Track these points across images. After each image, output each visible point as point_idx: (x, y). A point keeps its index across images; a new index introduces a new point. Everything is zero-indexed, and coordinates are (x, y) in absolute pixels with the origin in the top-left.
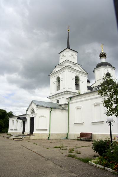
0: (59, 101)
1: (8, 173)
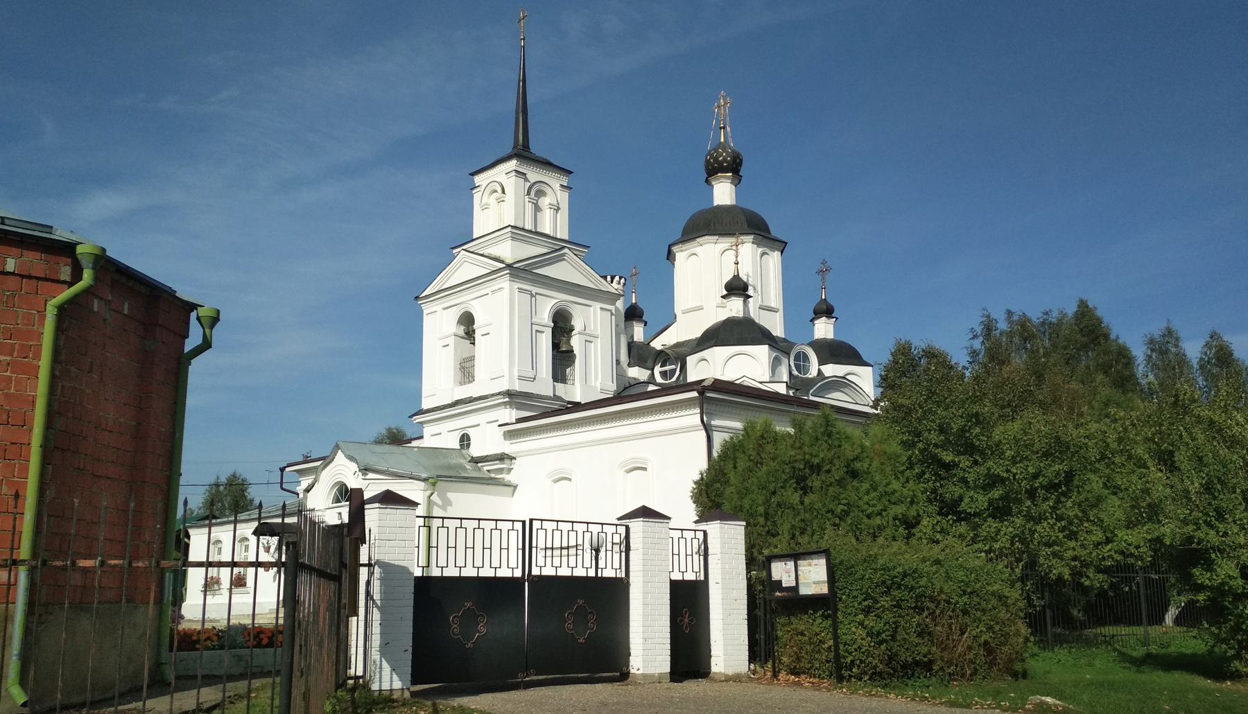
0: (469, 439)
1: (880, 435)
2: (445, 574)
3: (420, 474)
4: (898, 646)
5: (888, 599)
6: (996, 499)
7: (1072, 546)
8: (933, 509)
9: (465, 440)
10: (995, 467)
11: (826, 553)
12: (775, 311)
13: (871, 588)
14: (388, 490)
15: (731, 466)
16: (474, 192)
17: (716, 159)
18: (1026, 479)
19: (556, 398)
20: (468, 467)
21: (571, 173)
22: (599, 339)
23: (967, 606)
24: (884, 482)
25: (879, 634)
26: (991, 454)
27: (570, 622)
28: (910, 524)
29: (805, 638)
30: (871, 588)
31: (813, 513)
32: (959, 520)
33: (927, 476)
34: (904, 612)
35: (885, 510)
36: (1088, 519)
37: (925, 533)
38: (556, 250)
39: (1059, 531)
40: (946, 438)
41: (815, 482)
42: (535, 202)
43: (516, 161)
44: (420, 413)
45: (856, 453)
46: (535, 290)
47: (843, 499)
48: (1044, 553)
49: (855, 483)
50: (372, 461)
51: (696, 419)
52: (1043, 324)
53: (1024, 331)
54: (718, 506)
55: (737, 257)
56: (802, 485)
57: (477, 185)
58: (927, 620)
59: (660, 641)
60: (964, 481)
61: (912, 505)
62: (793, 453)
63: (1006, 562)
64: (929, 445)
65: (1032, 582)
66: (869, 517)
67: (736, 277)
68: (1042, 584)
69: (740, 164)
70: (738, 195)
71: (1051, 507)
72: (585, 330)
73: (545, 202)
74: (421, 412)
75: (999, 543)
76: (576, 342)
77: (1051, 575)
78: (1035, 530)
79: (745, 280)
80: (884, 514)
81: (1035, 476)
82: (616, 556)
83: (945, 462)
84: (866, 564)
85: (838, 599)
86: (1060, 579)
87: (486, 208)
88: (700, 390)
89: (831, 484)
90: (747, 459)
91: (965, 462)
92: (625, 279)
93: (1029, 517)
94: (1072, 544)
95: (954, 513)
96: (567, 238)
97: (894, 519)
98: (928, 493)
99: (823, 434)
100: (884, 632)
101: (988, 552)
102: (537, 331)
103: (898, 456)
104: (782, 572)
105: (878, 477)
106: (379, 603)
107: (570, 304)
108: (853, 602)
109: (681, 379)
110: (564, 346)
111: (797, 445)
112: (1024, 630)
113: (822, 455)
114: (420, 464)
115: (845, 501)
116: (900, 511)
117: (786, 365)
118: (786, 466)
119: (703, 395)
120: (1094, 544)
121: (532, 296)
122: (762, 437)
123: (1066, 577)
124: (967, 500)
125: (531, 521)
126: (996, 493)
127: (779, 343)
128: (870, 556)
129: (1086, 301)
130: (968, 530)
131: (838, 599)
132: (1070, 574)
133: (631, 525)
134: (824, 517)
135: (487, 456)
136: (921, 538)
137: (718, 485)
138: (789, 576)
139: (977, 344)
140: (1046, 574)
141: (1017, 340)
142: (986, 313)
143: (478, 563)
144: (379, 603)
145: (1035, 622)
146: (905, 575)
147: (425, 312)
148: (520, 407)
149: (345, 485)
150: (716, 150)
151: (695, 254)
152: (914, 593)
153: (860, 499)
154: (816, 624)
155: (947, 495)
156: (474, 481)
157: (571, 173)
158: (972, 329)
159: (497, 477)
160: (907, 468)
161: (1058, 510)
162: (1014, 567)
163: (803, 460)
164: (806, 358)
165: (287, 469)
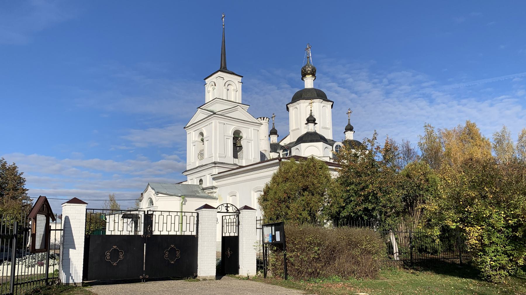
2: (161, 234)
14: (206, 204)
20: (200, 192)
22: (253, 141)
38: (235, 107)
50: (160, 191)
69: (315, 71)
70: (314, 84)
73: (231, 88)
74: (186, 171)
76: (243, 143)
82: (235, 227)
92: (269, 119)
107: (240, 128)
147: (188, 133)
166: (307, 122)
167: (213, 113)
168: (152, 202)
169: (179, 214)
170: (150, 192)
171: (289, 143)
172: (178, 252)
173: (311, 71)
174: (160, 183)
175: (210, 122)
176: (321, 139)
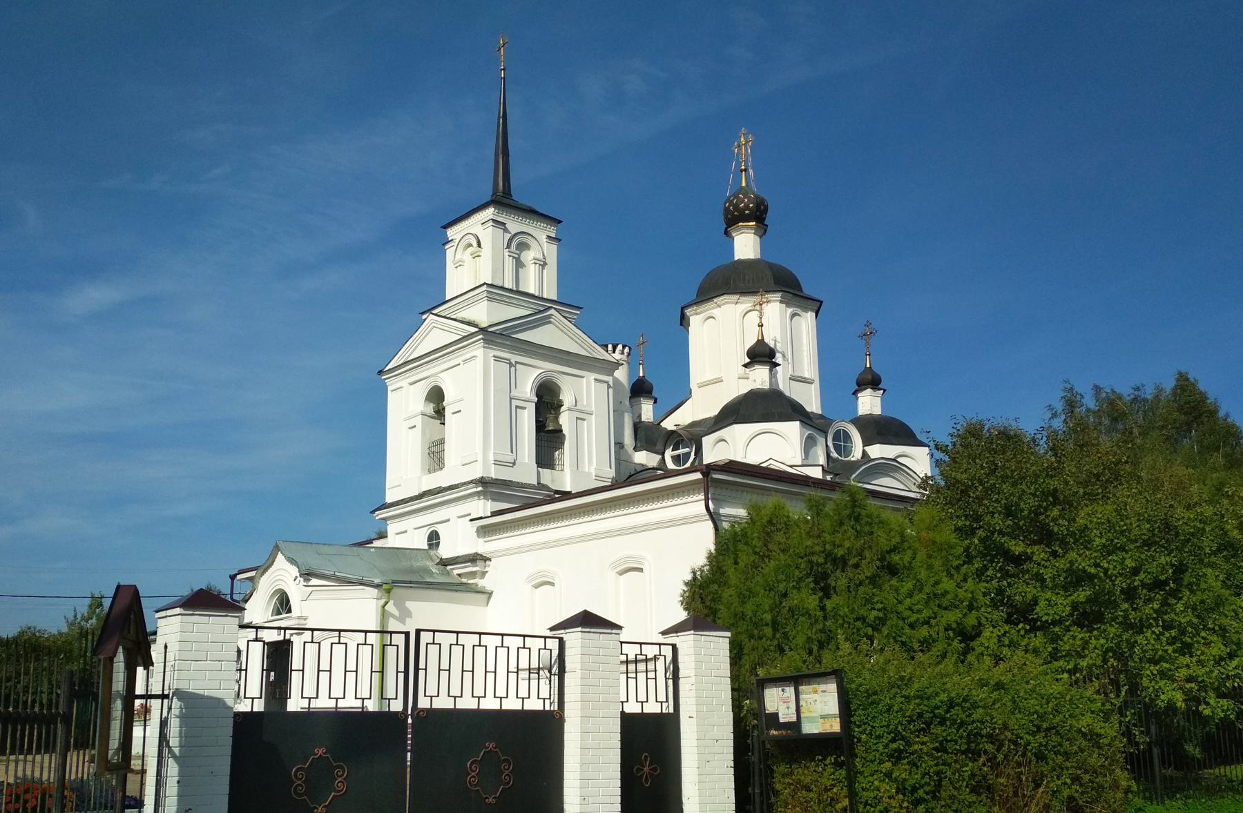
3: (373, 580)
4: (942, 806)
5: (926, 739)
6: (1081, 603)
7: (1185, 663)
8: (999, 615)
9: (434, 538)
10: (1079, 559)
11: (837, 674)
12: (810, 382)
13: (902, 724)
15: (730, 561)
16: (446, 247)
17: (736, 207)
18: (1121, 575)
19: (541, 486)
20: (434, 570)
21: (560, 222)
22: (593, 416)
23: (1043, 748)
24: (932, 580)
25: (914, 789)
26: (1074, 543)
27: (474, 774)
28: (968, 636)
29: (812, 795)
30: (902, 724)
31: (837, 621)
32: (1033, 629)
33: (990, 572)
34: (952, 757)
35: (935, 618)
36: (1205, 626)
37: (988, 648)
38: (541, 312)
39: (1168, 644)
40: (1014, 523)
41: (840, 580)
42: (517, 256)
43: (493, 209)
44: (384, 506)
45: (894, 542)
46: (514, 358)
47: (877, 602)
48: (1148, 672)
49: (894, 582)
50: (314, 563)
51: (700, 508)
52: (1135, 400)
53: (1114, 410)
54: (714, 612)
55: (761, 318)
56: (822, 585)
57: (450, 239)
58: (985, 769)
59: (606, 799)
60: (1040, 578)
61: (970, 612)
62: (809, 543)
63: (1097, 685)
64: (993, 533)
65: (1133, 711)
66: (912, 626)
67: (761, 342)
68: (1147, 713)
69: (766, 211)
71: (1155, 611)
72: (576, 405)
73: (529, 256)
75: (1087, 659)
76: (565, 420)
77: (1158, 702)
78: (1136, 642)
79: (772, 346)
80: (933, 622)
81: (1135, 571)
83: (1014, 554)
84: (894, 690)
85: (855, 740)
86: (1171, 707)
87: (460, 265)
88: (704, 471)
89: (861, 583)
90: (751, 551)
91: (1039, 553)
92: (630, 348)
93: (1127, 625)
94: (1186, 660)
95: (1026, 621)
96: (556, 298)
97: (946, 630)
98: (993, 595)
99: (849, 517)
100: (922, 786)
101: (1072, 672)
102: (517, 407)
103: (951, 547)
104: (778, 701)
105: (923, 574)
106: (176, 751)
107: (558, 376)
108: (876, 744)
109: (696, 464)
110: (551, 424)
111: (816, 532)
112: (1124, 778)
113: (847, 544)
114: (376, 567)
115: (880, 606)
116: (953, 619)
117: (822, 446)
118: (800, 560)
119: (707, 477)
120: (1214, 660)
121: (511, 365)
122: (770, 522)
123: (1179, 704)
124: (1042, 603)
125: (418, 632)
126: (1082, 595)
127: (814, 420)
128: (902, 678)
129: (1187, 373)
130: (1046, 643)
131: (855, 740)
132: (1184, 700)
133: (565, 637)
134: (852, 627)
135: (458, 557)
136: (982, 654)
137: (716, 587)
138: (788, 708)
139: (1058, 424)
140: (1151, 700)
141: (1106, 421)
142: (1068, 386)
143: (455, 691)
144: (176, 751)
145: (1138, 764)
146: (951, 705)
147: (390, 388)
148: (496, 497)
149: (286, 594)
150: (736, 196)
151: (714, 318)
152: (964, 731)
153: (900, 602)
154: (825, 774)
155: (1017, 598)
156: (439, 587)
157: (560, 222)
158: (1050, 406)
159: (469, 582)
160: (964, 563)
161: (1166, 615)
162: (1108, 691)
163: (823, 552)
164: (847, 437)
165: (239, 577)
166: (749, 360)
167: (477, 330)
168: (288, 601)
169: (372, 638)
170: (283, 574)
171: (690, 422)
172: (506, 767)
173: (755, 210)
174: (311, 543)
175: (468, 356)
176: (792, 411)
